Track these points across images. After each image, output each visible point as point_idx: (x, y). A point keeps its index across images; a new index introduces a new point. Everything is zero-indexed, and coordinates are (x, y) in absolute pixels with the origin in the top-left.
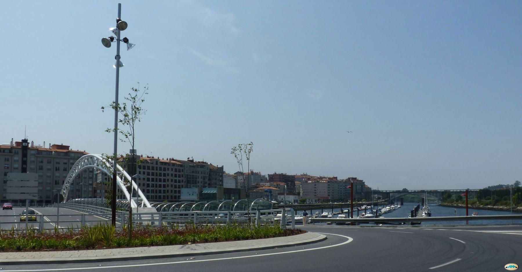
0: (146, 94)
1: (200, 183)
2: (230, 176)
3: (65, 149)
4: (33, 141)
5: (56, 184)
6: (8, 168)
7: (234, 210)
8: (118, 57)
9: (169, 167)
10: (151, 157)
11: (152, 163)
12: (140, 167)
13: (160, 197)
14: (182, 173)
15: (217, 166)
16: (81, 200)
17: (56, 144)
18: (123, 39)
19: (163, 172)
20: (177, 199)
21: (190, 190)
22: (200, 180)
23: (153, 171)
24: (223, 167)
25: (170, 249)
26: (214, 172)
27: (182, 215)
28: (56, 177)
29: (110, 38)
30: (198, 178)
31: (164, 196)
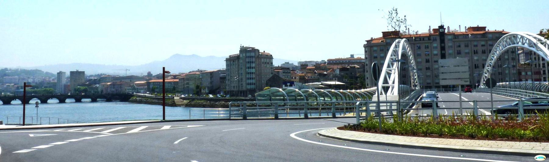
3: (481, 30)
4: (448, 27)
5: (476, 68)
6: (428, 54)
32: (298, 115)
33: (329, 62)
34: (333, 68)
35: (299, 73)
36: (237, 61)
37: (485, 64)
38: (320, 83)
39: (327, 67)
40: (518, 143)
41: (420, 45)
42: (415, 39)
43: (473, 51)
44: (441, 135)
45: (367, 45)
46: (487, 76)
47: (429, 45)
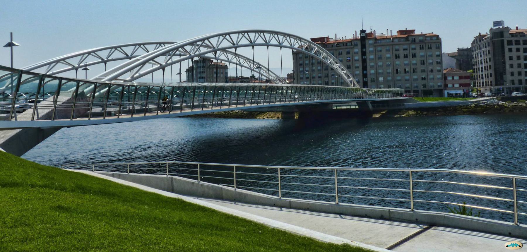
6: (350, 60)
28: (397, 65)
43: (394, 56)
47: (350, 50)
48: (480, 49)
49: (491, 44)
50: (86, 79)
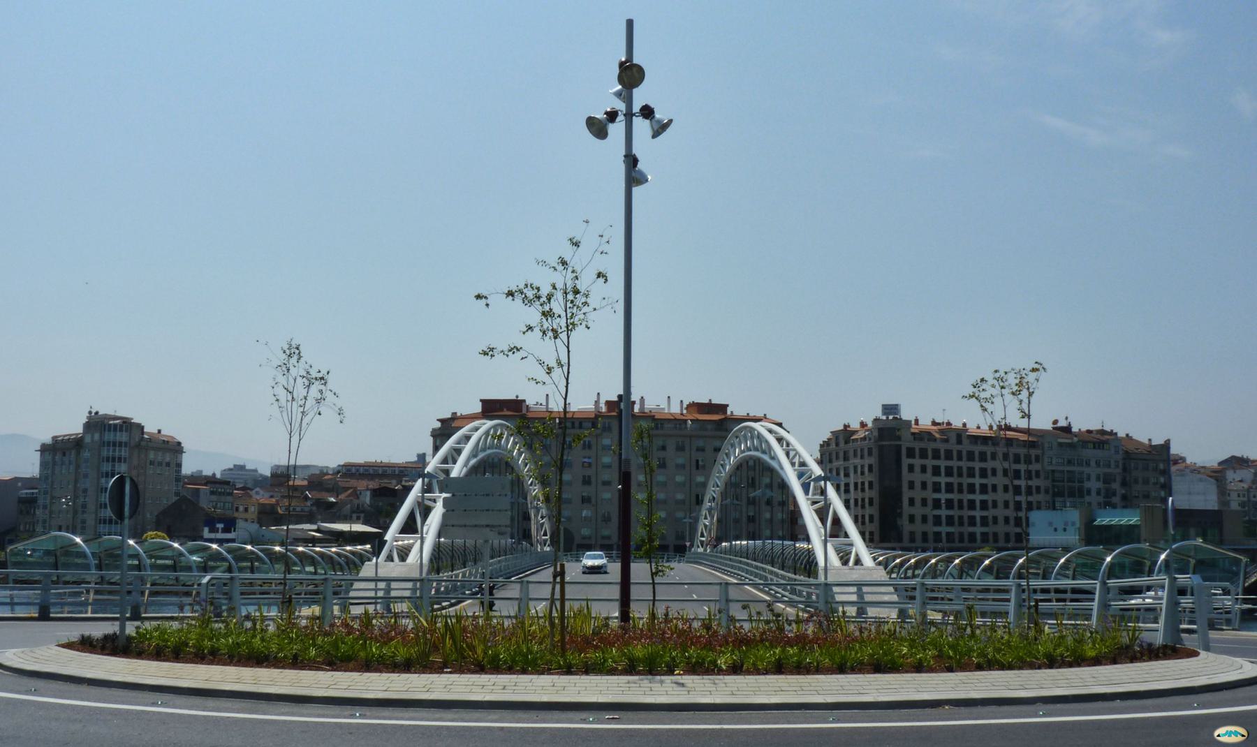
0: (602, 253)
1: (1094, 493)
2: (1199, 472)
3: (717, 413)
4: (642, 398)
6: (590, 464)
7: (1056, 579)
8: (631, 161)
9: (984, 448)
10: (943, 423)
11: (946, 441)
12: (911, 453)
13: (937, 536)
14: (1034, 467)
15: (1150, 440)
16: (731, 545)
17: (696, 402)
18: (640, 110)
19: (977, 465)
20: (966, 544)
21: (1056, 517)
22: (1093, 485)
23: (950, 463)
24: (1169, 444)
25: (786, 681)
26: (1141, 459)
27: (987, 590)
29: (607, 115)
30: (1089, 479)
31: (984, 535)
32: (9, 608)
33: (349, 470)
34: (356, 488)
35: (262, 497)
36: (73, 452)
37: (703, 496)
38: (314, 527)
39: (340, 483)
40: (321, 675)
41: (590, 439)
42: (560, 423)
44: (297, 662)
45: (438, 432)
46: (708, 524)
48: (846, 458)
49: (875, 451)
50: (550, 583)
